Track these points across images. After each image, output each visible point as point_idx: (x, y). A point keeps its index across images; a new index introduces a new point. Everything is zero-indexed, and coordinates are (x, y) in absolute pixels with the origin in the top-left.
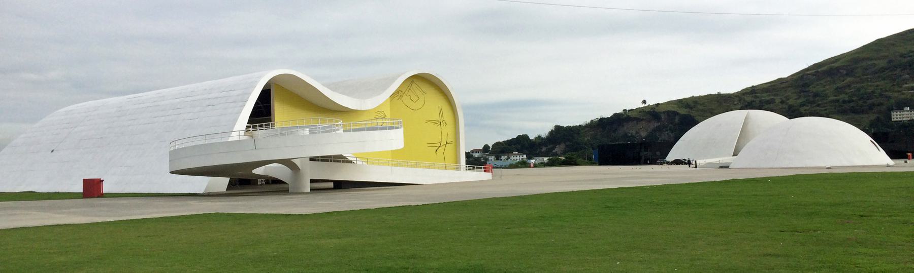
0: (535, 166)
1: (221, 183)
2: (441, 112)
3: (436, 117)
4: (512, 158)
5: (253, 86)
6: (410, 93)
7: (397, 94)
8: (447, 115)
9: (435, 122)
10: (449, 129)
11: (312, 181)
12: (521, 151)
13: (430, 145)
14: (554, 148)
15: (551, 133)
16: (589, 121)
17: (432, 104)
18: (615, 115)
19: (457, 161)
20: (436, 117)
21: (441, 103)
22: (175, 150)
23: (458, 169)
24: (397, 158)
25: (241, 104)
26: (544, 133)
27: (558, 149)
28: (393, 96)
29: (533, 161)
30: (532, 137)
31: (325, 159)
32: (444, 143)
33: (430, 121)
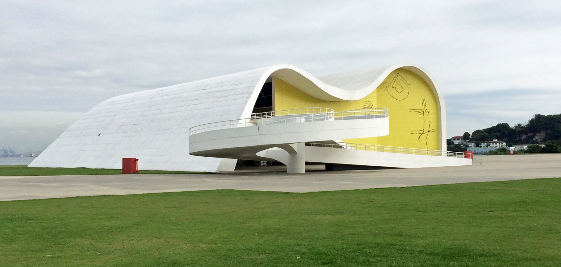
0: (515, 153)
2: (424, 102)
3: (419, 106)
4: (492, 145)
9: (418, 111)
10: (431, 118)
11: (307, 163)
12: (500, 139)
13: (414, 132)
15: (532, 122)
17: (416, 95)
19: (439, 147)
20: (419, 106)
21: (424, 93)
23: (439, 154)
24: (382, 143)
27: (537, 138)
28: (379, 87)
29: (512, 148)
30: (512, 125)
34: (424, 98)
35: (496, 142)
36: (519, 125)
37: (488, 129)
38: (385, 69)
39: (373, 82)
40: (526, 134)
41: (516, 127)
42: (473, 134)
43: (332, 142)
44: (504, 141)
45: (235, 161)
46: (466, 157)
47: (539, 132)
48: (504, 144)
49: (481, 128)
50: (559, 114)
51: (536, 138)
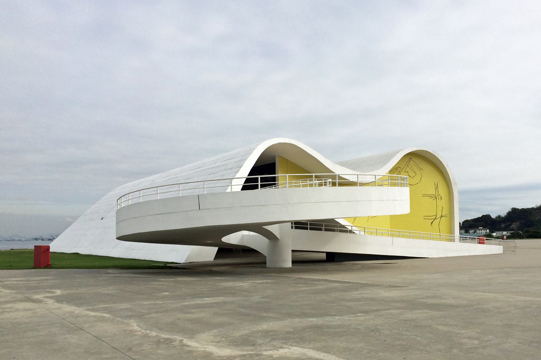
0: (498, 238)
1: (207, 254)
2: (437, 188)
3: (432, 191)
4: (478, 232)
5: (249, 153)
6: (408, 169)
7: (395, 170)
8: (442, 191)
9: (430, 196)
10: (443, 203)
11: (293, 251)
12: (484, 227)
13: (426, 217)
14: (511, 225)
15: (509, 213)
16: (531, 207)
17: (429, 180)
18: (483, 216)
19: (451, 231)
20: (432, 191)
21: (437, 178)
22: (121, 209)
23: (453, 240)
24: (398, 225)
25: (235, 170)
26: (503, 213)
27: (514, 226)
28: (391, 172)
29: (494, 234)
30: (493, 216)
31: (315, 226)
32: (439, 215)
33: (424, 195)
34: (436, 183)
35: (481, 230)
36: (499, 216)
37: (475, 219)
38: (397, 152)
39: (385, 164)
40: (504, 223)
41: (496, 217)
42: (463, 223)
43: (332, 221)
44: (488, 229)
45: (216, 249)
46: (480, 243)
47: (516, 222)
48: (488, 231)
49: (469, 218)
50: (539, 205)
51: (513, 226)
